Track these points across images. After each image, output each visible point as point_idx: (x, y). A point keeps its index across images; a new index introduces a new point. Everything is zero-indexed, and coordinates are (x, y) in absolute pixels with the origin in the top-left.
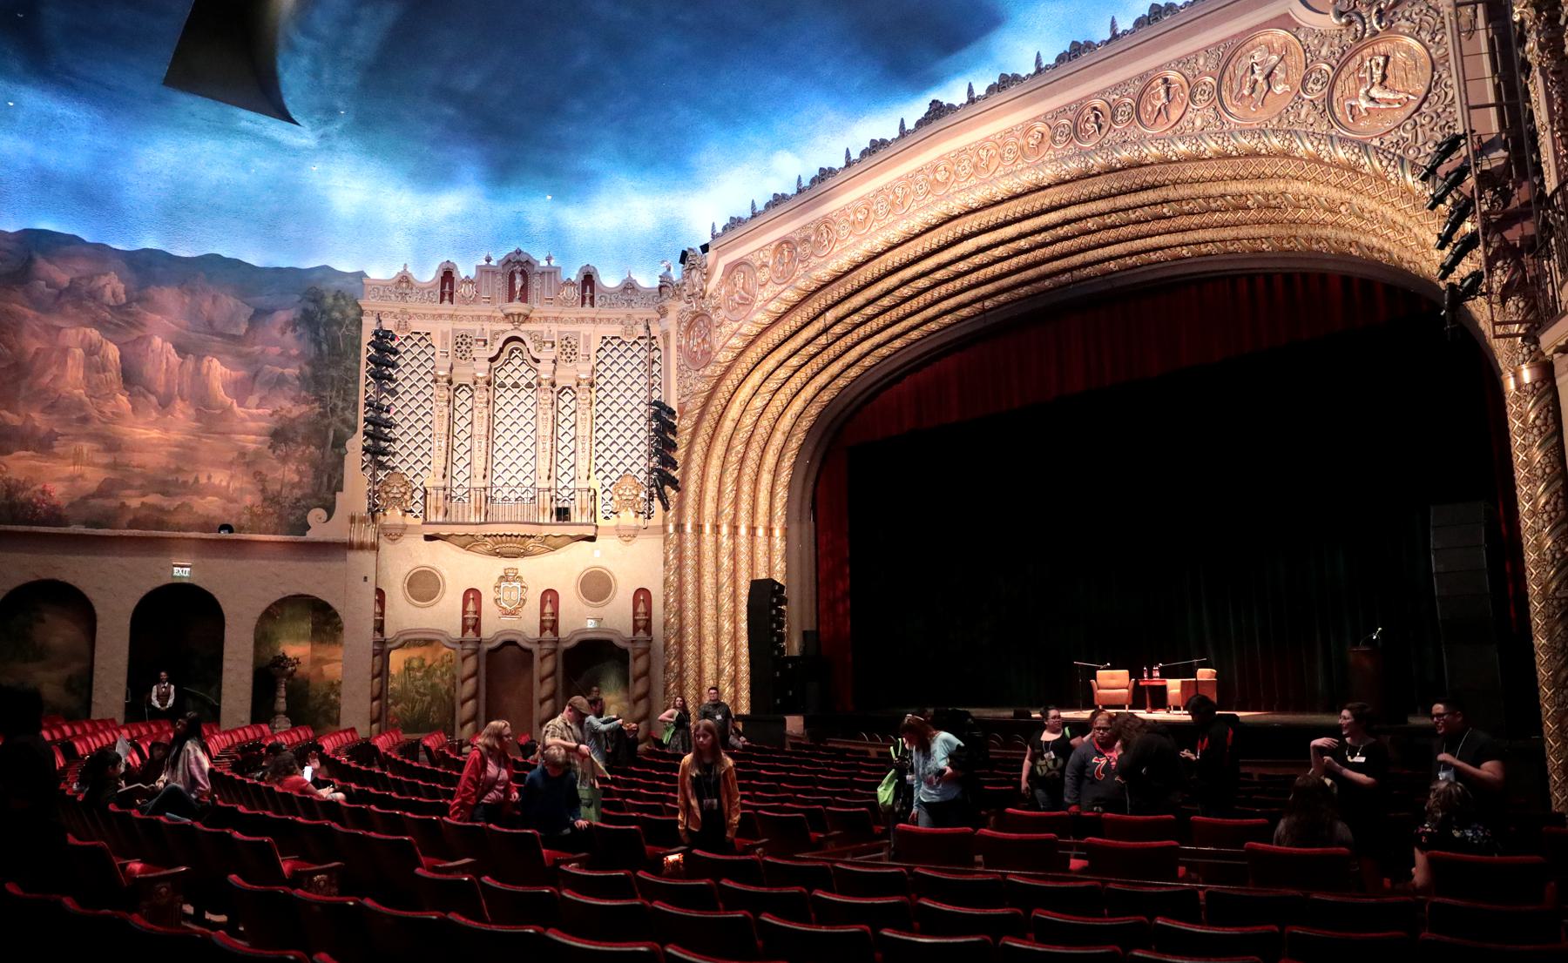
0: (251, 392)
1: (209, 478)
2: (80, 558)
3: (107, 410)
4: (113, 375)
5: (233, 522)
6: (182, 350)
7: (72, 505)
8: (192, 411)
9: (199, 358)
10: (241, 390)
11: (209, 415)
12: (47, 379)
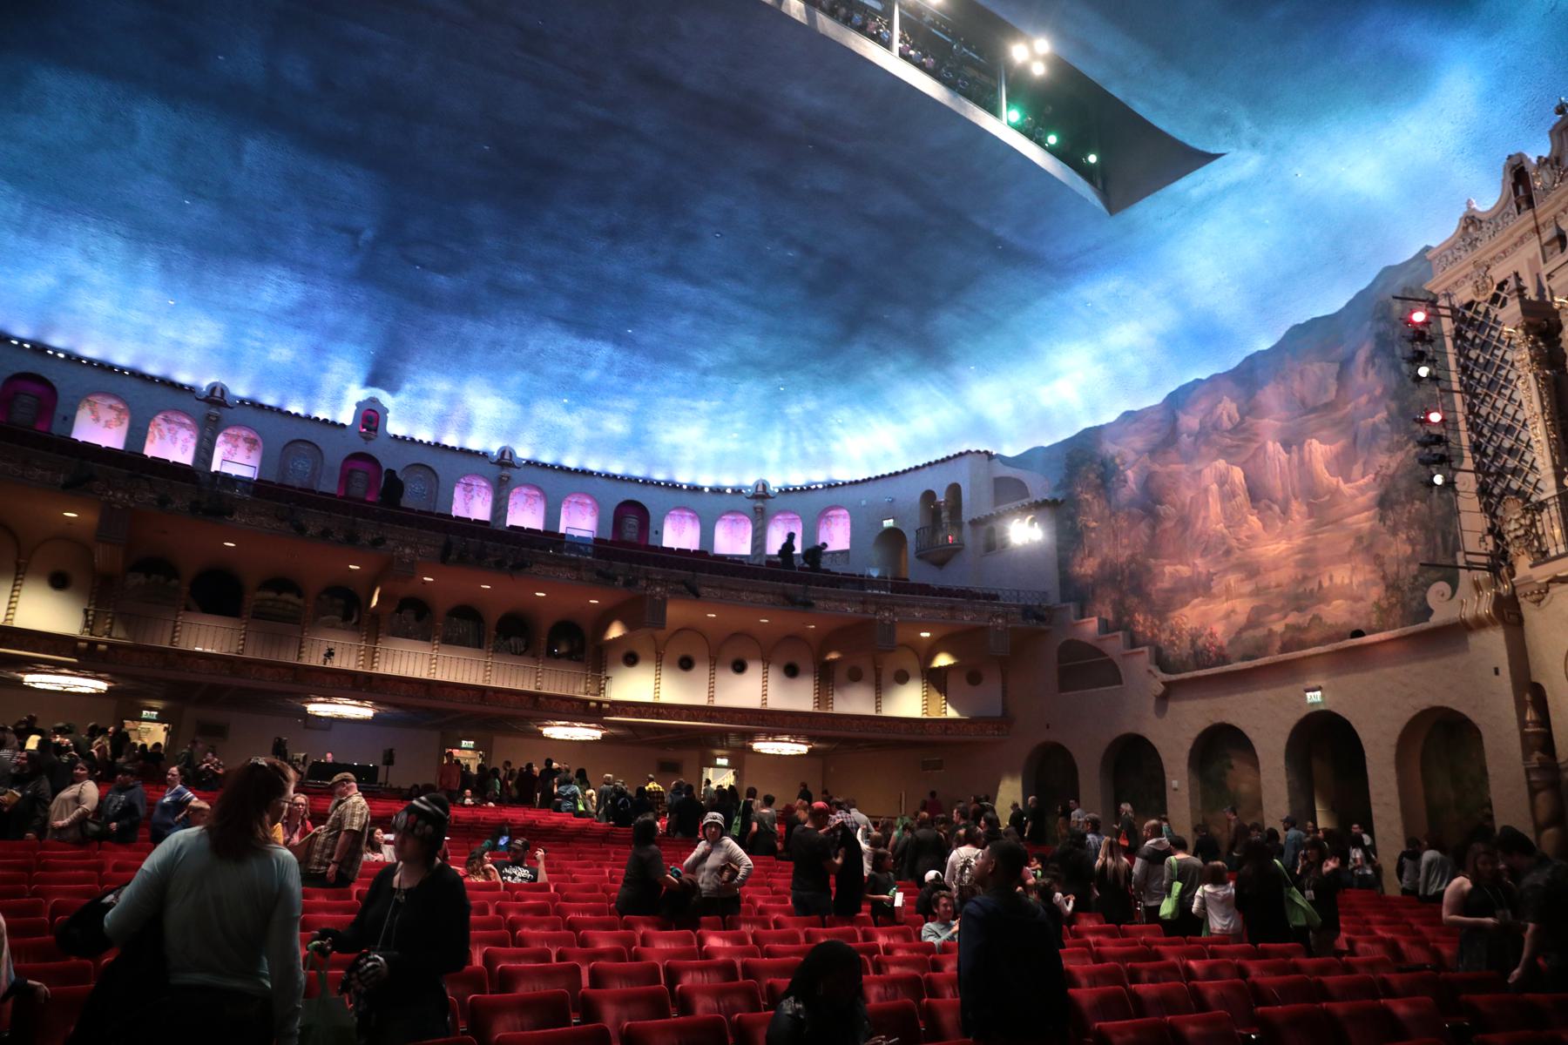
0: (1355, 462)
1: (1331, 578)
2: (1238, 696)
3: (1242, 536)
4: (1242, 498)
5: (1362, 625)
6: (1287, 446)
7: (1231, 643)
8: (1304, 509)
9: (1301, 446)
10: (1342, 465)
11: (1320, 506)
12: (1199, 525)
